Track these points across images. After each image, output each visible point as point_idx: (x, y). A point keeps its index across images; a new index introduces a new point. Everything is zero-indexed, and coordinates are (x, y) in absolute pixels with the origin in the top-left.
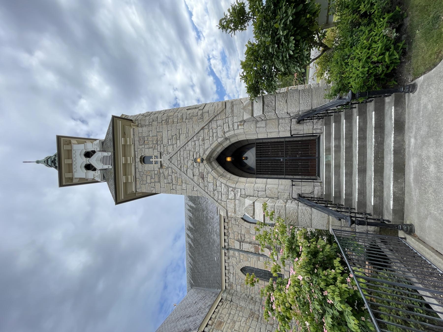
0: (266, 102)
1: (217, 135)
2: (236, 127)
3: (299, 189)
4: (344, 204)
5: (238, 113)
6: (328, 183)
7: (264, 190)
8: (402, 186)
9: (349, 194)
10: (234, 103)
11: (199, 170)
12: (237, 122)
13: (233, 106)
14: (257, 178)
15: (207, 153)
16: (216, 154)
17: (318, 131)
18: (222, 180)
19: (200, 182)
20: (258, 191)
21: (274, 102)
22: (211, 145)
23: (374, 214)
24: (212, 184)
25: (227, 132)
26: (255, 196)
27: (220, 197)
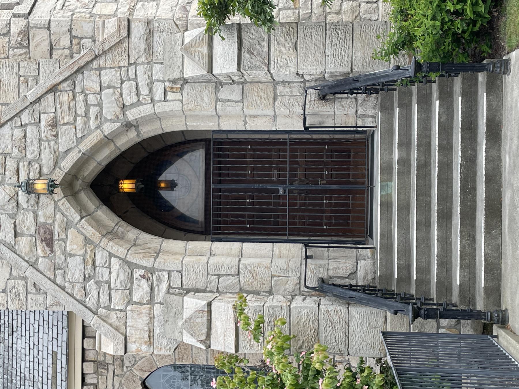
0: (246, 43)
1: (101, 111)
2: (158, 94)
3: (321, 266)
4: (414, 293)
5: (167, 55)
6: (387, 248)
7: (234, 271)
8: (497, 243)
9: (424, 270)
10: (156, 25)
11: (36, 218)
12: (163, 81)
13: (150, 34)
14: (213, 240)
15: (67, 164)
16: (91, 170)
17: (369, 122)
18: (114, 247)
19: (40, 253)
20: (219, 276)
21: (265, 44)
22: (79, 141)
23: (461, 302)
24: (79, 259)
25: (132, 106)
26: (209, 290)
27: (104, 298)
